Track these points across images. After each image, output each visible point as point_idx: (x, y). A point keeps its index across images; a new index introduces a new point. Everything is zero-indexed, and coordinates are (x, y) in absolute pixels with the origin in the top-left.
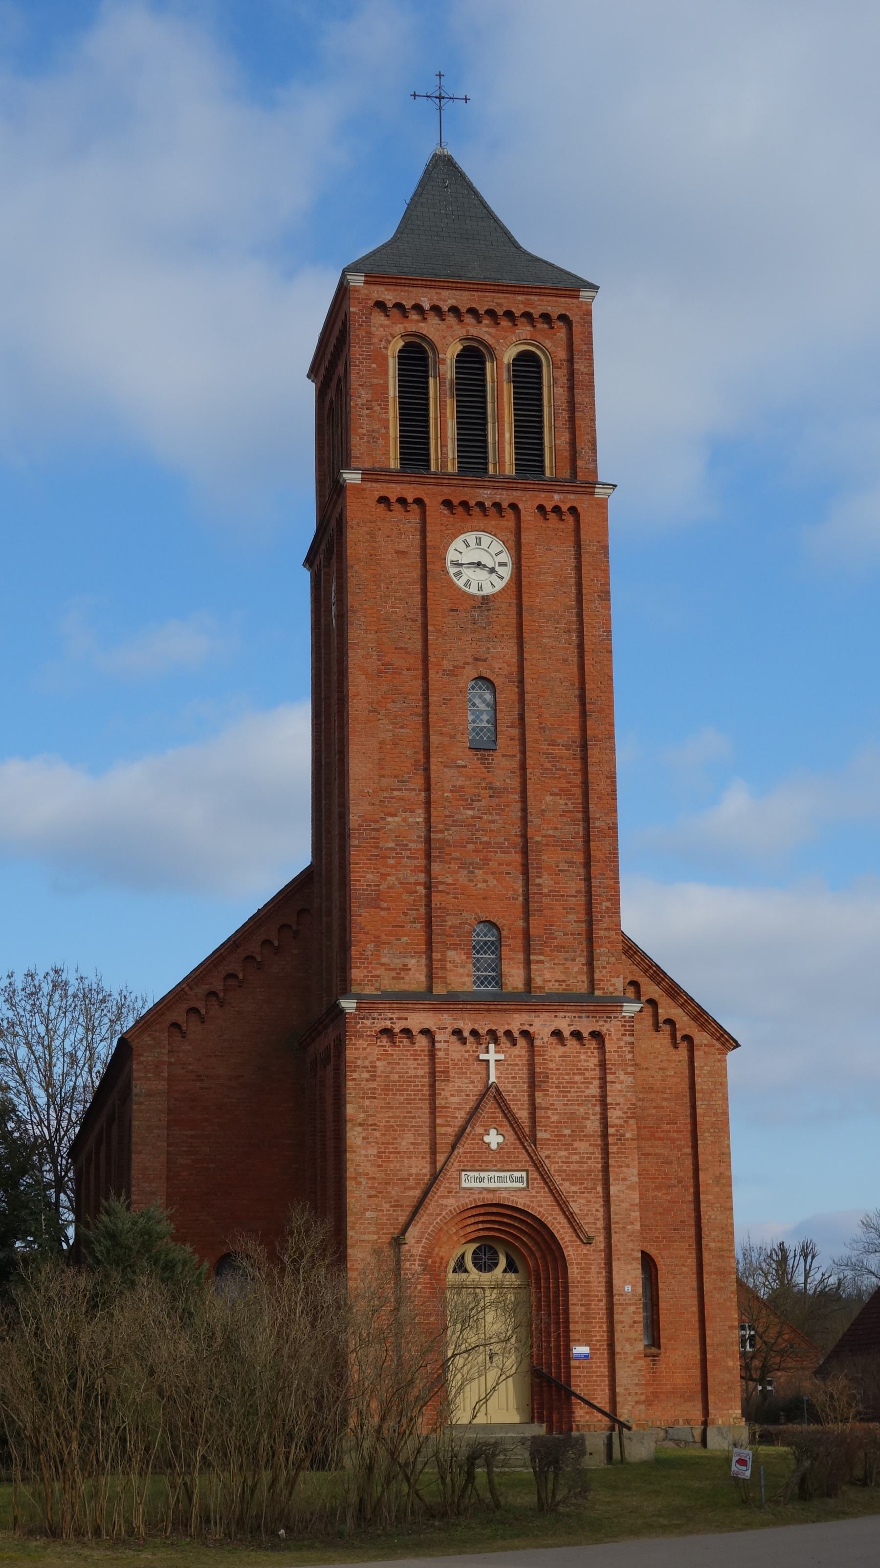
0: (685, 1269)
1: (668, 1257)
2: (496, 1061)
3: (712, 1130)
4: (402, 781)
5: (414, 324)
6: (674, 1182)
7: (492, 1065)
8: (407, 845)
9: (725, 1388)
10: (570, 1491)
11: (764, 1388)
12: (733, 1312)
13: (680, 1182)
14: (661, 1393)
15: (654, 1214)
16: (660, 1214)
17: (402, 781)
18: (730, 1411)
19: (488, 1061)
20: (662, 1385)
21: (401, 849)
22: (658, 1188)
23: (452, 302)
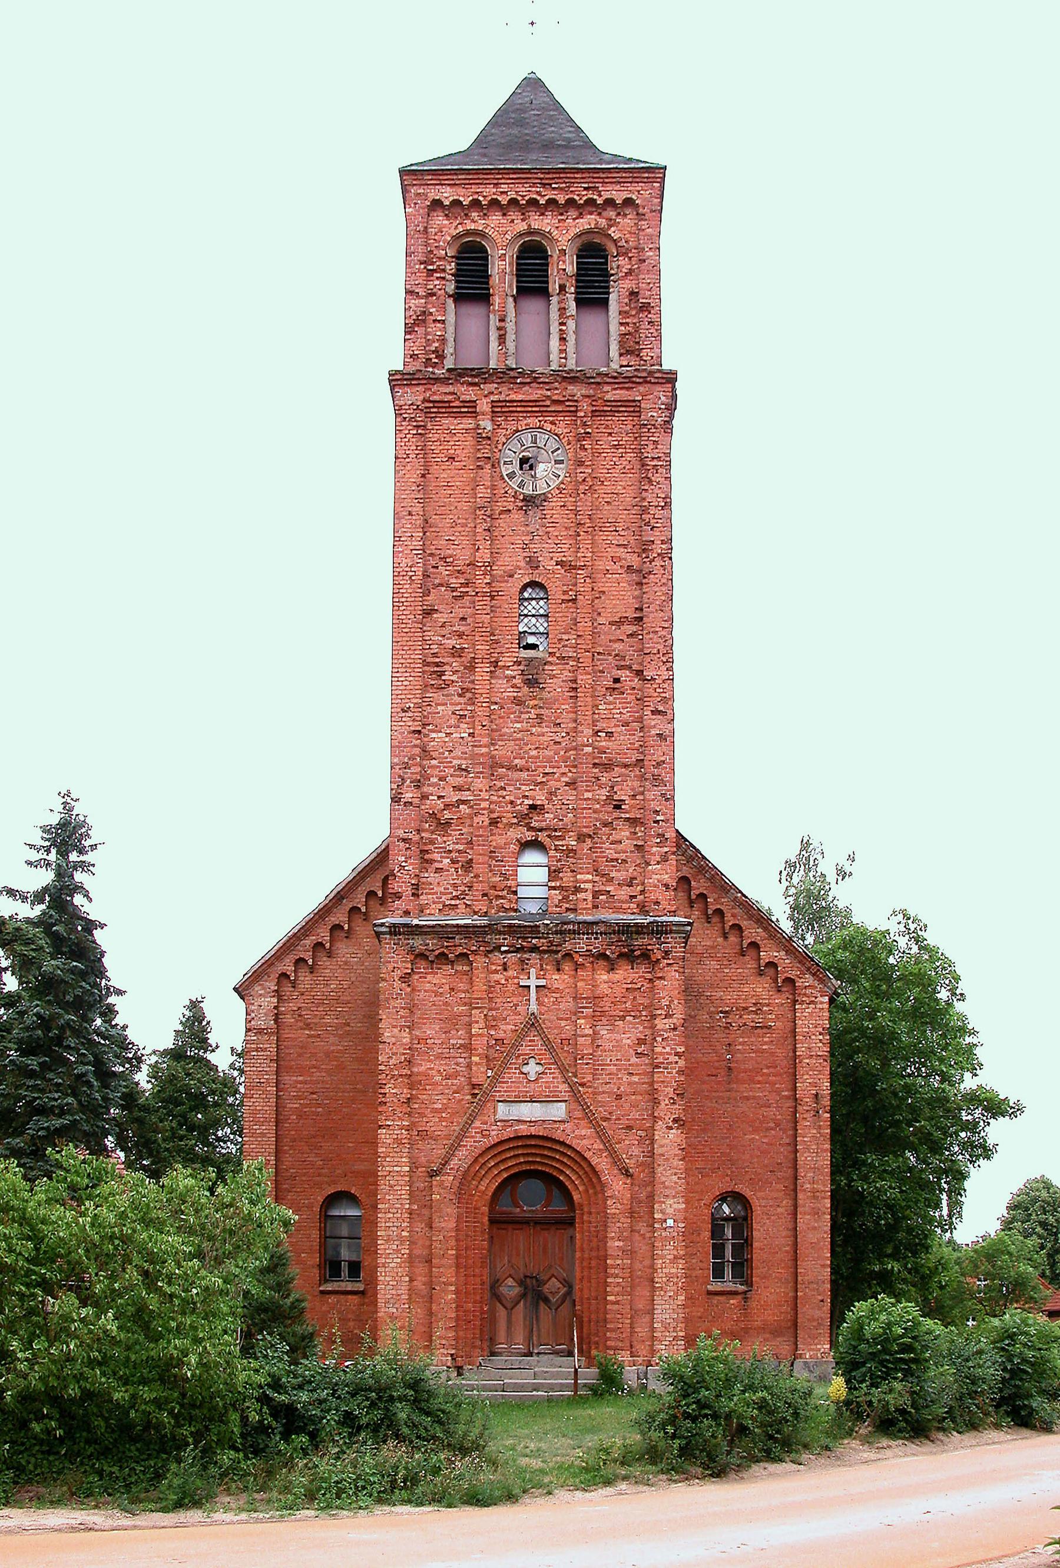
0: (779, 1210)
1: (763, 1199)
2: (537, 987)
3: (811, 1073)
4: (447, 695)
5: (588, 221)
6: (772, 1125)
7: (533, 990)
8: (451, 762)
9: (815, 1324)
10: (191, 1256)
11: (207, 1095)
12: (825, 1251)
13: (777, 1125)
14: (751, 1328)
15: (751, 1156)
16: (758, 1157)
17: (447, 695)
18: (819, 1347)
19: (529, 987)
20: (754, 1321)
21: (445, 767)
22: (756, 1130)
23: (625, 195)
